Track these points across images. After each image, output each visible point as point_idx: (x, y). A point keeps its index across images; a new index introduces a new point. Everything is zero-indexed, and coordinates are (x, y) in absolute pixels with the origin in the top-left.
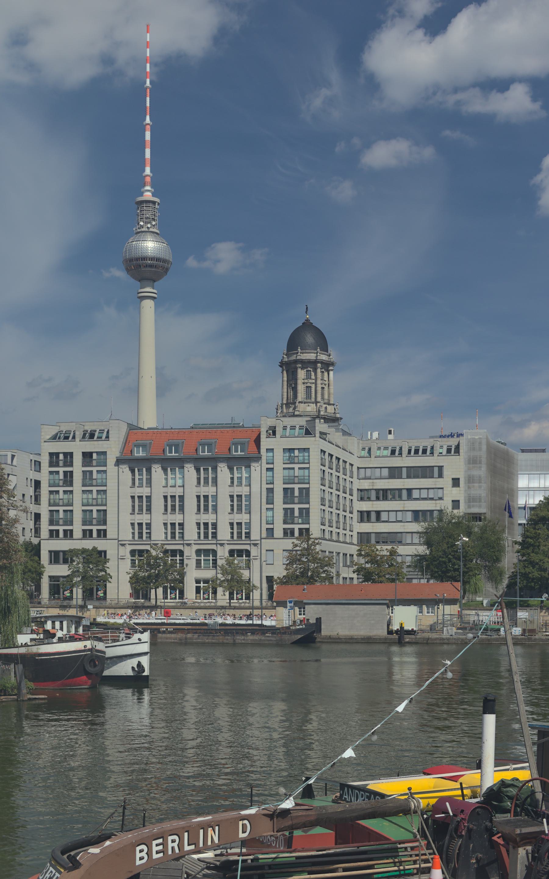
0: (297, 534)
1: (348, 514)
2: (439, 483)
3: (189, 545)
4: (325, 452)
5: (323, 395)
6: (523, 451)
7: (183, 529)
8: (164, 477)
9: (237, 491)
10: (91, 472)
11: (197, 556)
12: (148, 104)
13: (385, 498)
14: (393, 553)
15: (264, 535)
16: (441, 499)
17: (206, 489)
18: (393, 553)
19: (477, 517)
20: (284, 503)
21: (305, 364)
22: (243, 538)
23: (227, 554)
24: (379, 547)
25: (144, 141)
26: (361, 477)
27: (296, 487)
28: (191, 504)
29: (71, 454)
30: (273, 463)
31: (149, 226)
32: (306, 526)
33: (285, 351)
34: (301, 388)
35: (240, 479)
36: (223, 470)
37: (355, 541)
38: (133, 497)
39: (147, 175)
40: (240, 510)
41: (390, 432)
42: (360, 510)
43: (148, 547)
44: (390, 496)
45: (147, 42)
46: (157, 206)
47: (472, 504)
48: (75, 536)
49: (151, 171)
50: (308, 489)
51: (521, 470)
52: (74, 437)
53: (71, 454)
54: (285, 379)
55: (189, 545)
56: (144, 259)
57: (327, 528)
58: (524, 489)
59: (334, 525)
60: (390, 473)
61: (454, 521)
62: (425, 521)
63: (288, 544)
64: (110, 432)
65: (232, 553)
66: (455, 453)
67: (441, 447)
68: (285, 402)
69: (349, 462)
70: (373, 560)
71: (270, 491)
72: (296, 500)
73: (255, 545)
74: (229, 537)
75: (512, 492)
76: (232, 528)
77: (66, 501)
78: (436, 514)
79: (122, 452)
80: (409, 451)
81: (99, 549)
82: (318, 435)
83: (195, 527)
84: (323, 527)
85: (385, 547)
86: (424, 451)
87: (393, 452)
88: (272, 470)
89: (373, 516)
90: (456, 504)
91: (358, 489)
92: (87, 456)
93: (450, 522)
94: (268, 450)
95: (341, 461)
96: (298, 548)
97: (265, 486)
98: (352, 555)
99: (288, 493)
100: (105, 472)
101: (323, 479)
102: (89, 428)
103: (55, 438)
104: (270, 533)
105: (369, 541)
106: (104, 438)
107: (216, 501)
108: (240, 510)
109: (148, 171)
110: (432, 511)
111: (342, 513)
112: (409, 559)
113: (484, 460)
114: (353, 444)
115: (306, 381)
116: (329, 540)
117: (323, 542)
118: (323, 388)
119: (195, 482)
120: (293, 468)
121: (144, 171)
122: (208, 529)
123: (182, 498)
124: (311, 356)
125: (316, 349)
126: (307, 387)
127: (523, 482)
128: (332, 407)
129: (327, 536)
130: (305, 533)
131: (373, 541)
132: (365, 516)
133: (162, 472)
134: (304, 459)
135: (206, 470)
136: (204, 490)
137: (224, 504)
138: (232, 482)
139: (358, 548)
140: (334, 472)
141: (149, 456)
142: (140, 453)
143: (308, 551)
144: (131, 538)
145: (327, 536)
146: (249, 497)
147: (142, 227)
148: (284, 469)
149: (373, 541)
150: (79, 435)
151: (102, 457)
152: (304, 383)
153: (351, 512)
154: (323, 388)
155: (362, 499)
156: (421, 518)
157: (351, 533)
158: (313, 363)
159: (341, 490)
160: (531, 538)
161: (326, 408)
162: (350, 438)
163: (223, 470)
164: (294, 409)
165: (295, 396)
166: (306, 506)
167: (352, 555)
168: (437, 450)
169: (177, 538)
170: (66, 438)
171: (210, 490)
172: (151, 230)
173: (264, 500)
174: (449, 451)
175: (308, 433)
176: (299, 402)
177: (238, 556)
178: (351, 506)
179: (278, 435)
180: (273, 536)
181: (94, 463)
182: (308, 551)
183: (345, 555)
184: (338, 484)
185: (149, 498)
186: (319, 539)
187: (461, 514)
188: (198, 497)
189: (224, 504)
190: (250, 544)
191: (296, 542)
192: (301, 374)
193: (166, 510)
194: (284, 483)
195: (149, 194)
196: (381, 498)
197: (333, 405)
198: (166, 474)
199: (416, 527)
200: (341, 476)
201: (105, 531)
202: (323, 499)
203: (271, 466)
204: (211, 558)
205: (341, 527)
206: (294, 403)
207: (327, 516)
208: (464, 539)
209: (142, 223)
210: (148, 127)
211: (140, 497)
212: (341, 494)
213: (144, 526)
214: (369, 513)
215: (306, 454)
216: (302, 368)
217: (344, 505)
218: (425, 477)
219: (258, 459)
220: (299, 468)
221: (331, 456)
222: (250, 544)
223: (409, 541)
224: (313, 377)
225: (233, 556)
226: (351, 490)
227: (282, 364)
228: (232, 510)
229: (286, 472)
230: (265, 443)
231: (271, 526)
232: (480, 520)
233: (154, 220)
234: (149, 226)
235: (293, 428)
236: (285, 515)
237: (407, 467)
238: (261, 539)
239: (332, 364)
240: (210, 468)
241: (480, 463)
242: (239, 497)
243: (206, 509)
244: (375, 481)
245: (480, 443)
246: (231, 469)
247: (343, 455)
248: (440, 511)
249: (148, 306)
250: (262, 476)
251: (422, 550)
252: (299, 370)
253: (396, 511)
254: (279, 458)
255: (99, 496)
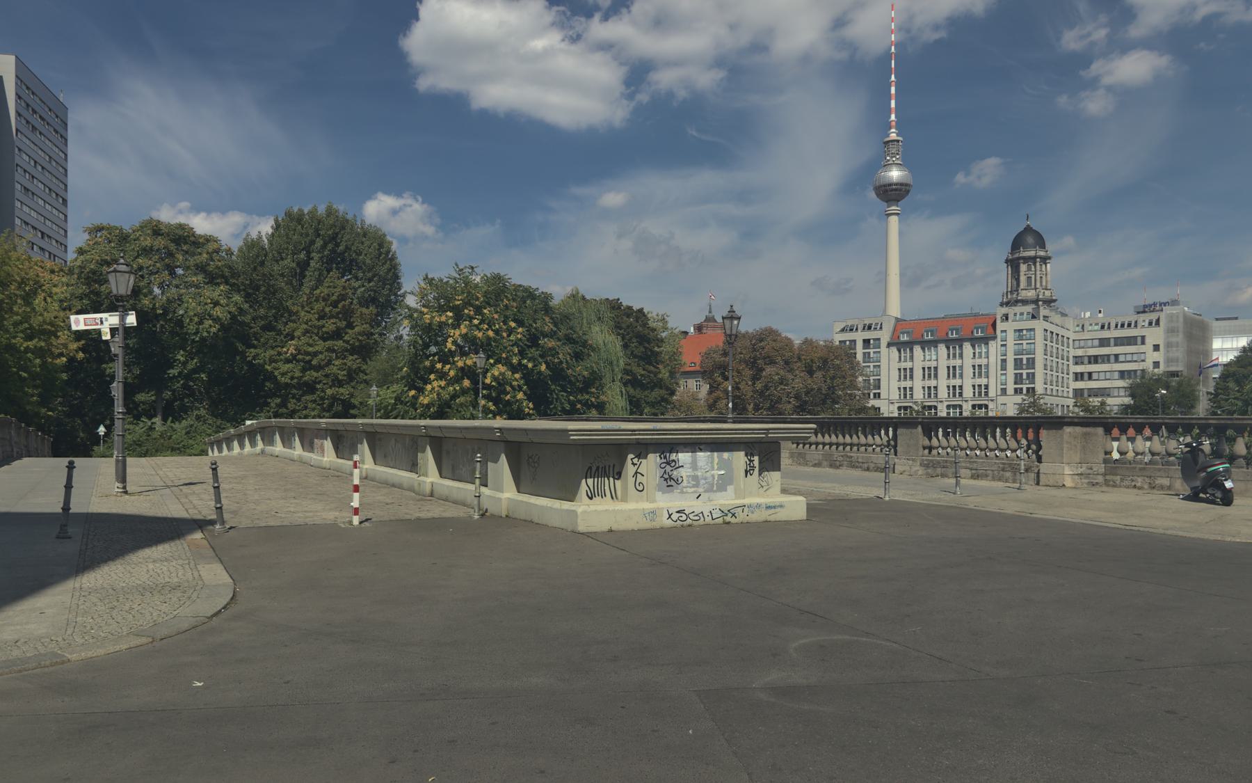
0: (1025, 391)
1: (1065, 376)
2: (1142, 348)
3: (941, 402)
4: (1047, 330)
5: (1041, 282)
6: (1217, 319)
7: (937, 391)
8: (922, 354)
9: (978, 361)
10: (869, 353)
11: (947, 409)
12: (893, 66)
13: (1096, 362)
14: (1103, 403)
15: (999, 393)
16: (1143, 361)
17: (955, 361)
18: (1103, 403)
19: (1174, 374)
20: (1015, 369)
21: (1026, 260)
22: (983, 395)
23: (970, 408)
24: (1091, 400)
25: (890, 94)
26: (1076, 347)
27: (1025, 357)
28: (943, 372)
29: (855, 341)
30: (1006, 341)
31: (894, 159)
32: (1032, 386)
33: (1010, 251)
34: (1023, 279)
35: (980, 353)
36: (967, 348)
37: (1071, 395)
38: (899, 369)
39: (893, 121)
40: (980, 375)
41: (1100, 312)
42: (1075, 371)
43: (910, 404)
44: (1100, 361)
45: (892, 18)
46: (900, 144)
47: (1170, 364)
48: (1008, 393)
49: (896, 117)
50: (1034, 359)
51: (1215, 335)
52: (857, 329)
53: (855, 341)
54: (1010, 272)
55: (941, 402)
56: (890, 185)
57: (1049, 387)
58: (1217, 350)
59: (1055, 384)
60: (1100, 342)
61: (1154, 378)
62: (1130, 378)
63: (1018, 399)
64: (883, 324)
65: (974, 407)
66: (1156, 325)
67: (1144, 321)
68: (1009, 290)
69: (1060, 334)
70: (1087, 410)
71: (1004, 361)
72: (1024, 367)
73: (992, 400)
74: (972, 396)
75: (1207, 352)
76: (974, 389)
77: (875, 373)
78: (1139, 373)
79: (891, 338)
80: (1117, 326)
81: (876, 406)
82: (1041, 318)
83: (946, 389)
84: (1046, 386)
85: (1096, 399)
86: (1129, 325)
87: (1103, 327)
88: (1005, 345)
89: (1086, 376)
90: (1156, 364)
91: (1073, 357)
92: (866, 342)
93: (1151, 379)
94: (1002, 331)
95: (1060, 336)
96: (1026, 402)
97: (1000, 358)
98: (1068, 406)
99: (1018, 363)
100: (879, 352)
101: (1046, 350)
102: (867, 322)
103: (843, 330)
104: (1004, 391)
105: (1082, 395)
106: (878, 329)
107: (962, 370)
108: (980, 375)
109: (893, 117)
110: (1135, 371)
111: (1060, 375)
112: (1116, 408)
113: (1181, 329)
114: (1070, 323)
115: (1027, 273)
116: (1050, 395)
117: (1047, 397)
118: (1041, 277)
119: (946, 356)
120: (1022, 344)
121: (890, 117)
122: (955, 390)
123: (936, 368)
124: (1032, 253)
125: (1036, 247)
126: (1028, 277)
127: (1217, 344)
128: (1049, 292)
129: (1049, 392)
130: (1031, 391)
131: (1086, 395)
132: (1079, 377)
133: (921, 351)
134: (1031, 337)
135: (954, 348)
136: (952, 363)
137: (968, 371)
138: (974, 356)
139: (1074, 400)
140: (1054, 344)
141: (911, 340)
142: (905, 338)
143: (1034, 404)
144: (898, 398)
145: (1049, 392)
146: (987, 366)
147: (889, 160)
148: (1015, 344)
149: (1086, 395)
150: (860, 327)
151: (877, 342)
152: (1025, 275)
153: (1068, 374)
154: (1041, 277)
155: (1076, 363)
156: (1126, 376)
157: (1068, 390)
158: (1033, 259)
159: (1060, 358)
160: (1221, 389)
161: (1044, 293)
162: (1066, 318)
163: (967, 348)
164: (1018, 295)
165: (1018, 285)
166: (1033, 371)
167: (1068, 406)
168: (1140, 324)
169: (932, 397)
170: (851, 330)
171: (958, 362)
172: (895, 162)
173: (999, 368)
174: (1150, 324)
175: (1034, 317)
176: (1022, 290)
177: (979, 409)
178: (1068, 369)
179: (1010, 320)
180: (1006, 393)
181: (872, 346)
182: (1034, 404)
183: (1063, 406)
184: (1057, 353)
185: (911, 370)
186: (1043, 394)
187: (1161, 372)
188: (948, 367)
189: (968, 371)
190: (988, 400)
191: (1024, 397)
192: (1023, 267)
193: (924, 377)
194: (1015, 355)
195: (894, 135)
196: (1093, 362)
197: (1050, 289)
198: (924, 351)
199: (1121, 383)
200: (1060, 347)
201: (879, 394)
202: (1045, 365)
203: (1004, 343)
204: (958, 411)
205: (1060, 385)
206: (1018, 291)
207: (1049, 378)
208: (1163, 391)
209: (888, 158)
210: (893, 83)
211: (905, 369)
212: (1060, 360)
213: (908, 389)
214: (1082, 374)
215: (1032, 333)
216: (1024, 263)
217: (1062, 369)
218: (1128, 345)
219: (994, 338)
220: (1027, 344)
221: (1052, 333)
222: (988, 400)
223: (1116, 394)
224: (1033, 269)
225: (975, 409)
226: (1068, 357)
227: (1007, 261)
228: (974, 375)
229: (1016, 346)
230: (1000, 326)
231: (1004, 387)
232: (1178, 376)
233: (898, 154)
234: (894, 159)
235: (1022, 314)
236: (1016, 378)
237: (1115, 338)
238: (997, 396)
239: (1050, 258)
240: (957, 347)
241: (1178, 332)
242: (980, 366)
243: (954, 376)
244: (1087, 349)
245: (1178, 317)
246: (973, 347)
247: (1061, 332)
248: (1143, 371)
249: (894, 220)
250: (29, 137)
251: (1128, 401)
252: (1022, 265)
253: (1106, 372)
254: (1011, 336)
255: (875, 370)
